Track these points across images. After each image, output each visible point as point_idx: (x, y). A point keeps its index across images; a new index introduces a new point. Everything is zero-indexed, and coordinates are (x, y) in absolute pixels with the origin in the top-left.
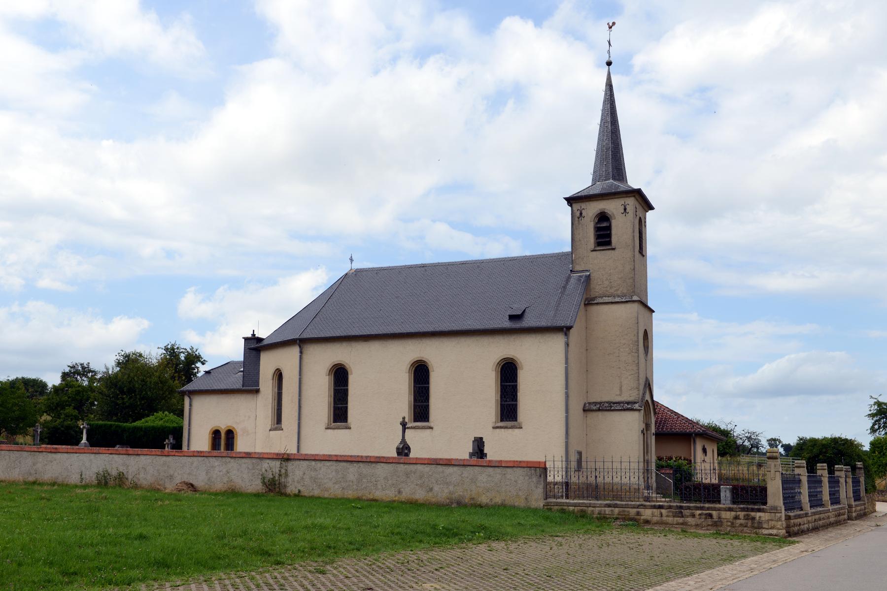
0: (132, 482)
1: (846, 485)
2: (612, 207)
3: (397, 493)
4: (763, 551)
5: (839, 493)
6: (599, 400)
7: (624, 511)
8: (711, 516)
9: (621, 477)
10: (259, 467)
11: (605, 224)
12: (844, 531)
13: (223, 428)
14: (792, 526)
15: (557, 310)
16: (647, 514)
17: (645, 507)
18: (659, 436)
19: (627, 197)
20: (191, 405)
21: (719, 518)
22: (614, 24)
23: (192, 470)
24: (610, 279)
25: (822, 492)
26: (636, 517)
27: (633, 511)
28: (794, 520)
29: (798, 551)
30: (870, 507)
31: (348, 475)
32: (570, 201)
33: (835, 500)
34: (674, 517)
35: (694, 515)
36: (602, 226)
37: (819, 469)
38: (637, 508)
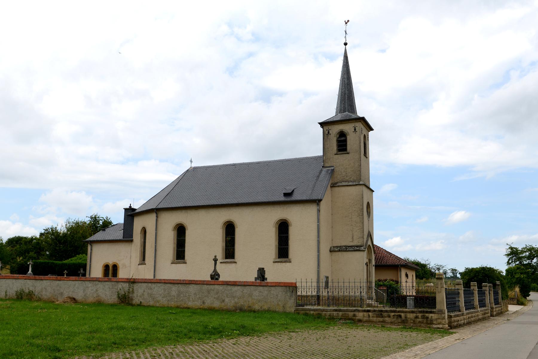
0: (38, 297)
1: (489, 295)
2: (347, 128)
3: (202, 303)
4: (430, 340)
5: (485, 300)
6: (339, 245)
7: (345, 314)
8: (400, 316)
9: (301, 291)
10: (116, 287)
11: (343, 139)
12: (487, 324)
13: (111, 263)
14: (453, 322)
15: (313, 190)
16: (360, 315)
17: (359, 311)
18: (378, 267)
19: (356, 122)
20: (91, 250)
21: (406, 317)
22: (348, 21)
23: (75, 289)
24: (346, 172)
25: (474, 300)
26: (353, 317)
27: (351, 314)
28: (454, 318)
29: (453, 340)
30: (505, 308)
31: (171, 292)
32: (322, 124)
33: (482, 304)
34: (377, 317)
35: (390, 316)
36: (341, 139)
37: (472, 286)
38: (354, 312)
